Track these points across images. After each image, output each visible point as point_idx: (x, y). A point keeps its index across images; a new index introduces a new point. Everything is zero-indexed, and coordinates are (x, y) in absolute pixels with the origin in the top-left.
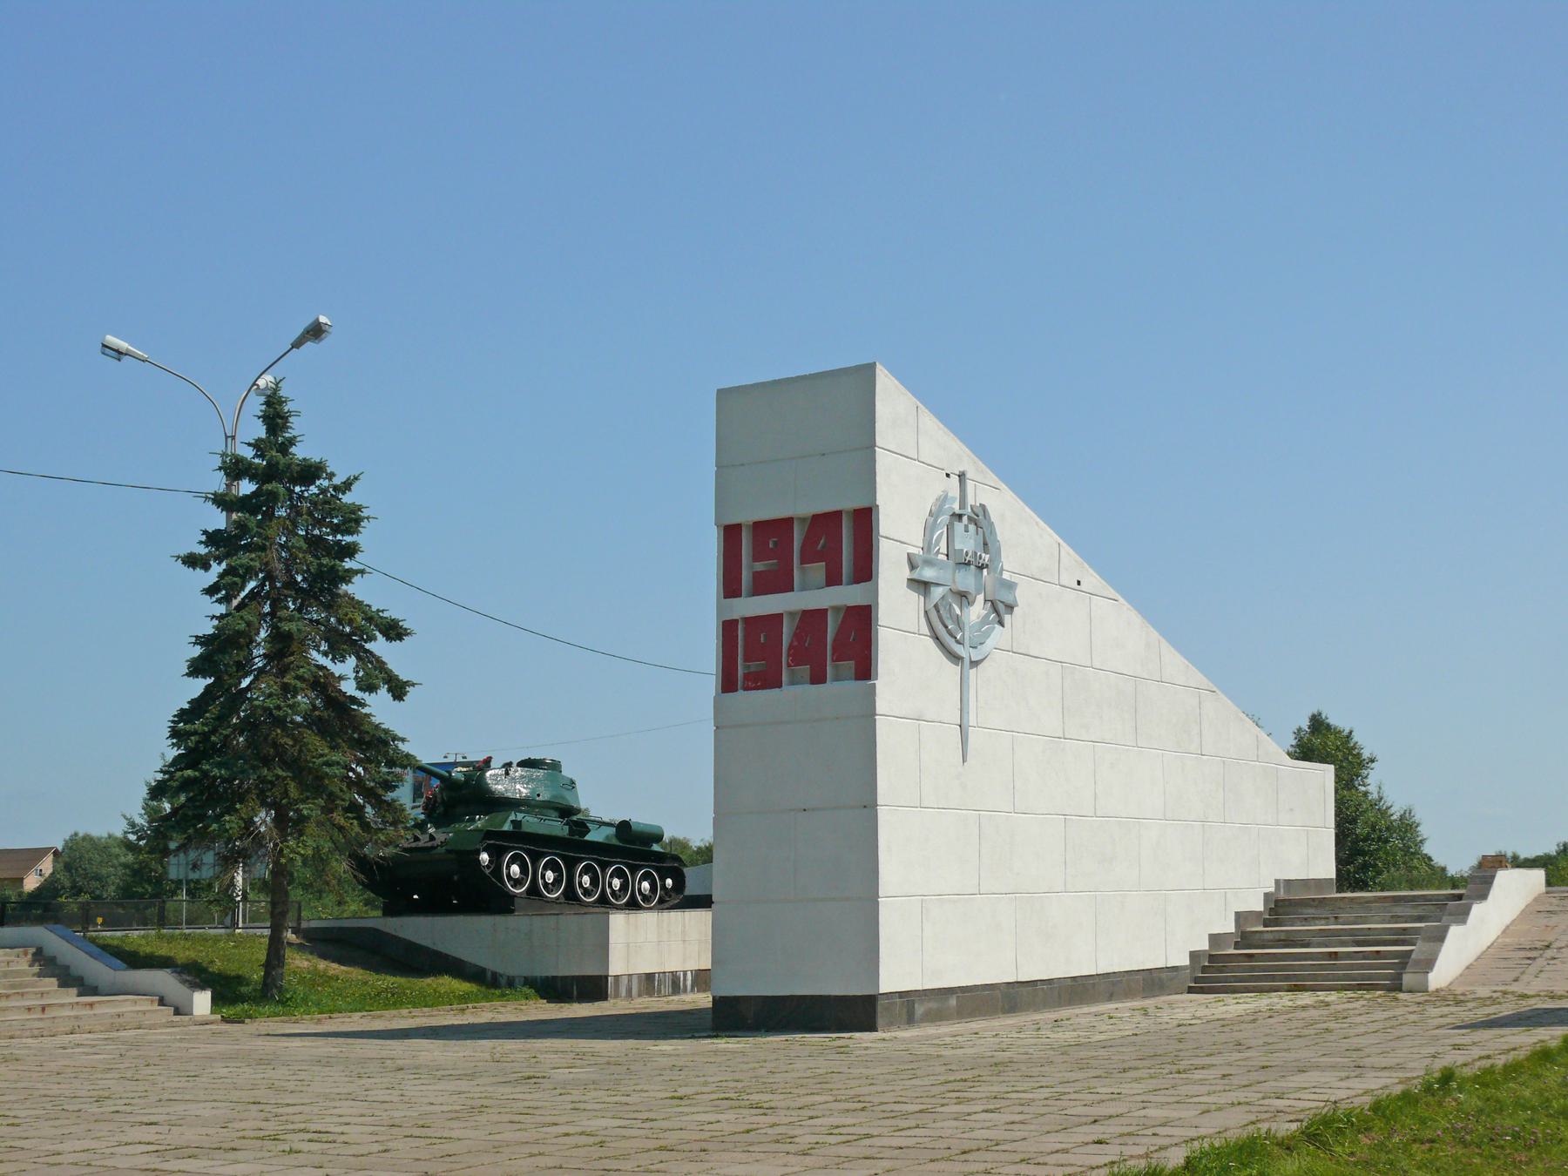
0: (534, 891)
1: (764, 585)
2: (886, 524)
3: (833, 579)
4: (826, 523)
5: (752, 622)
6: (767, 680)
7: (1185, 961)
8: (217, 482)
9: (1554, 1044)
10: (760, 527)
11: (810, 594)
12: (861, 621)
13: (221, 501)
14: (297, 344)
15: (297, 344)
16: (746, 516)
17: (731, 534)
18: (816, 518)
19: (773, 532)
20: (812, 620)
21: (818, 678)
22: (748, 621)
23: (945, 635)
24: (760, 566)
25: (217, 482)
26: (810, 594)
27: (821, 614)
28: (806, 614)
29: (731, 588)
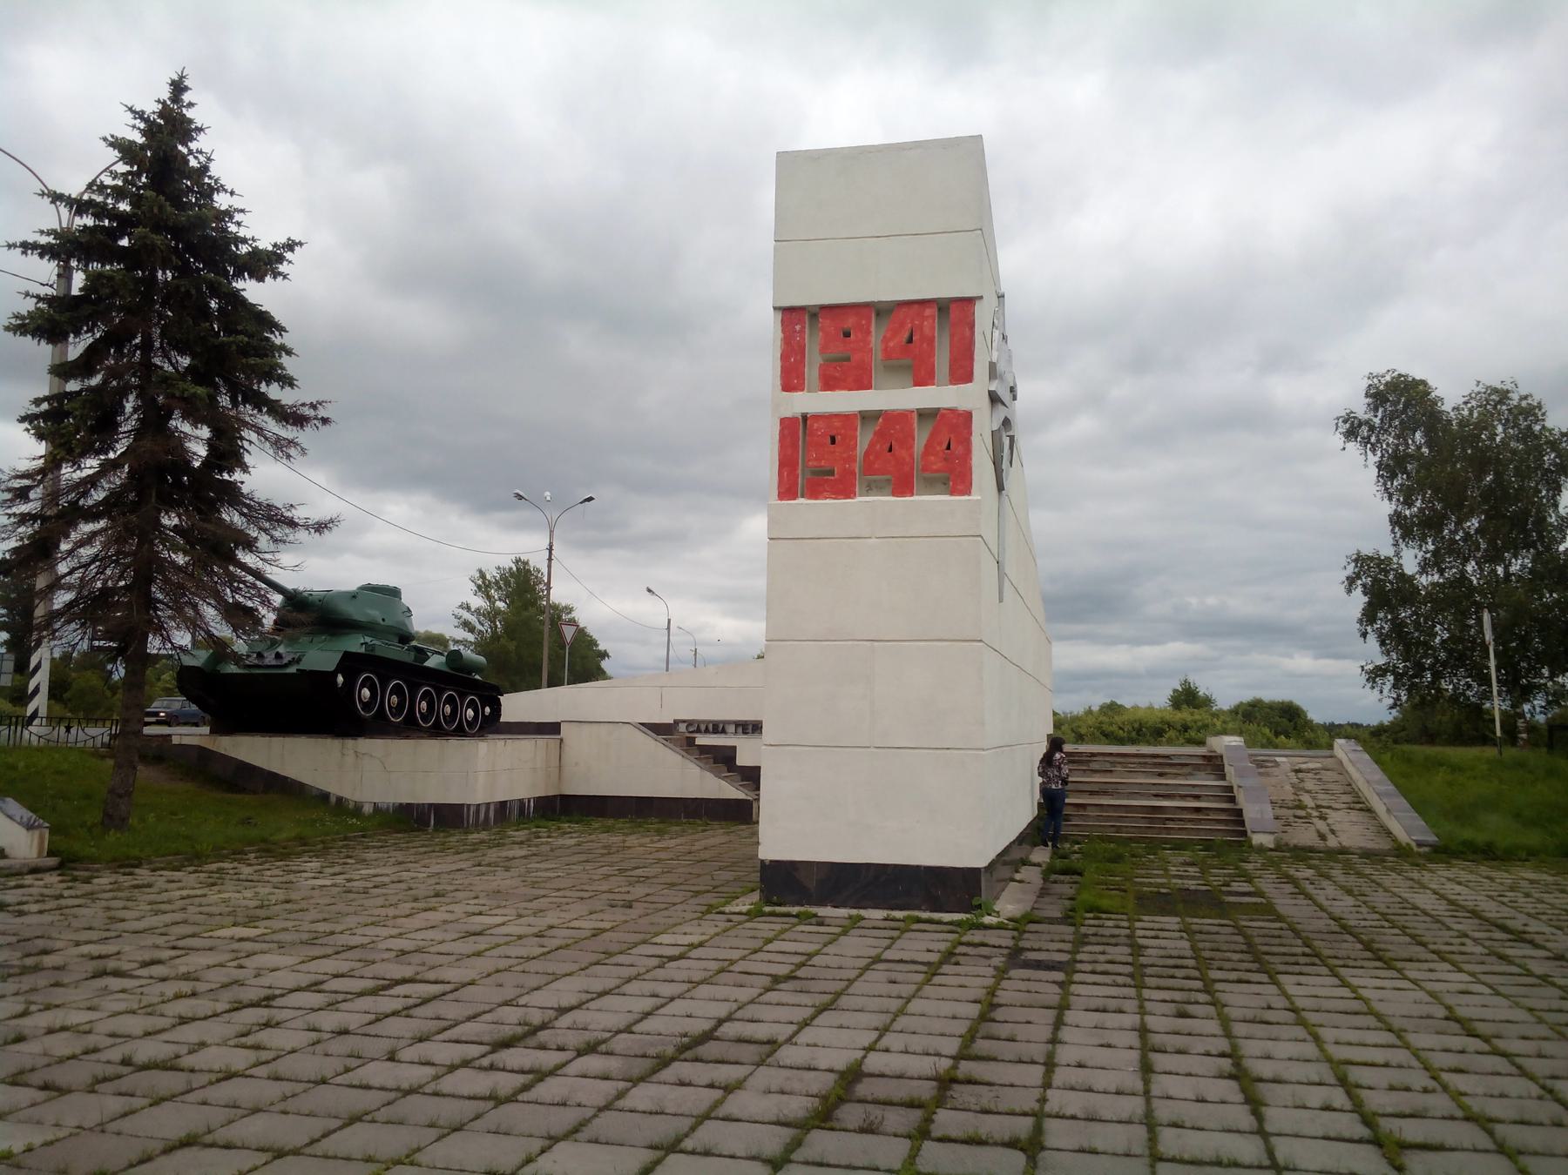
0: (437, 725)
17: (790, 315)
20: (891, 425)
29: (791, 379)
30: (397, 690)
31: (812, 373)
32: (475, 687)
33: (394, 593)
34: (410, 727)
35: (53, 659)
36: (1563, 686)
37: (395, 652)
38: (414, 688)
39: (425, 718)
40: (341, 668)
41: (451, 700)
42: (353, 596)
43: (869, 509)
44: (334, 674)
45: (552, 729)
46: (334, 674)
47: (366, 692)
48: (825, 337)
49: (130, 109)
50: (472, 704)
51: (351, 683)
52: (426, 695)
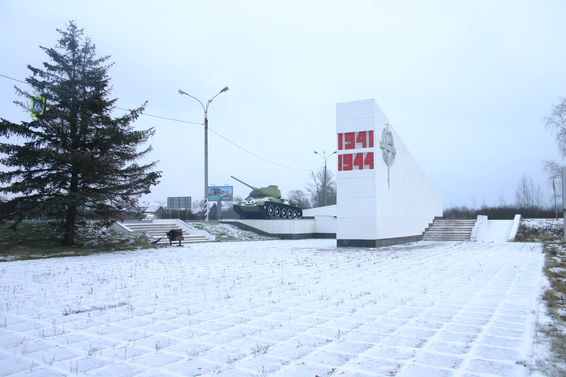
0: (274, 215)
1: (348, 147)
2: (375, 134)
3: (364, 146)
4: (362, 134)
5: (345, 155)
6: (350, 168)
7: (544, 255)
8: (53, 42)
9: (126, 162)
10: (347, 134)
11: (358, 149)
12: (370, 156)
13: (53, 54)
14: (221, 92)
15: (221, 92)
16: (344, 131)
17: (340, 135)
18: (360, 132)
19: (350, 136)
20: (360, 155)
21: (361, 168)
22: (344, 155)
23: (386, 160)
24: (346, 143)
25: (53, 42)
26: (358, 149)
27: (362, 154)
28: (358, 154)
29: (340, 148)
30: (278, 209)
31: (344, 146)
32: (296, 208)
33: (276, 187)
34: (281, 217)
35: (40, 176)
36: (8, 154)
37: (277, 201)
38: (281, 209)
39: (284, 215)
40: (265, 205)
41: (290, 211)
42: (267, 188)
43: (356, 171)
44: (264, 206)
45: (313, 218)
46: (264, 206)
47: (271, 210)
48: (347, 139)
49: (115, 100)
50: (295, 212)
51: (267, 208)
52: (284, 210)
